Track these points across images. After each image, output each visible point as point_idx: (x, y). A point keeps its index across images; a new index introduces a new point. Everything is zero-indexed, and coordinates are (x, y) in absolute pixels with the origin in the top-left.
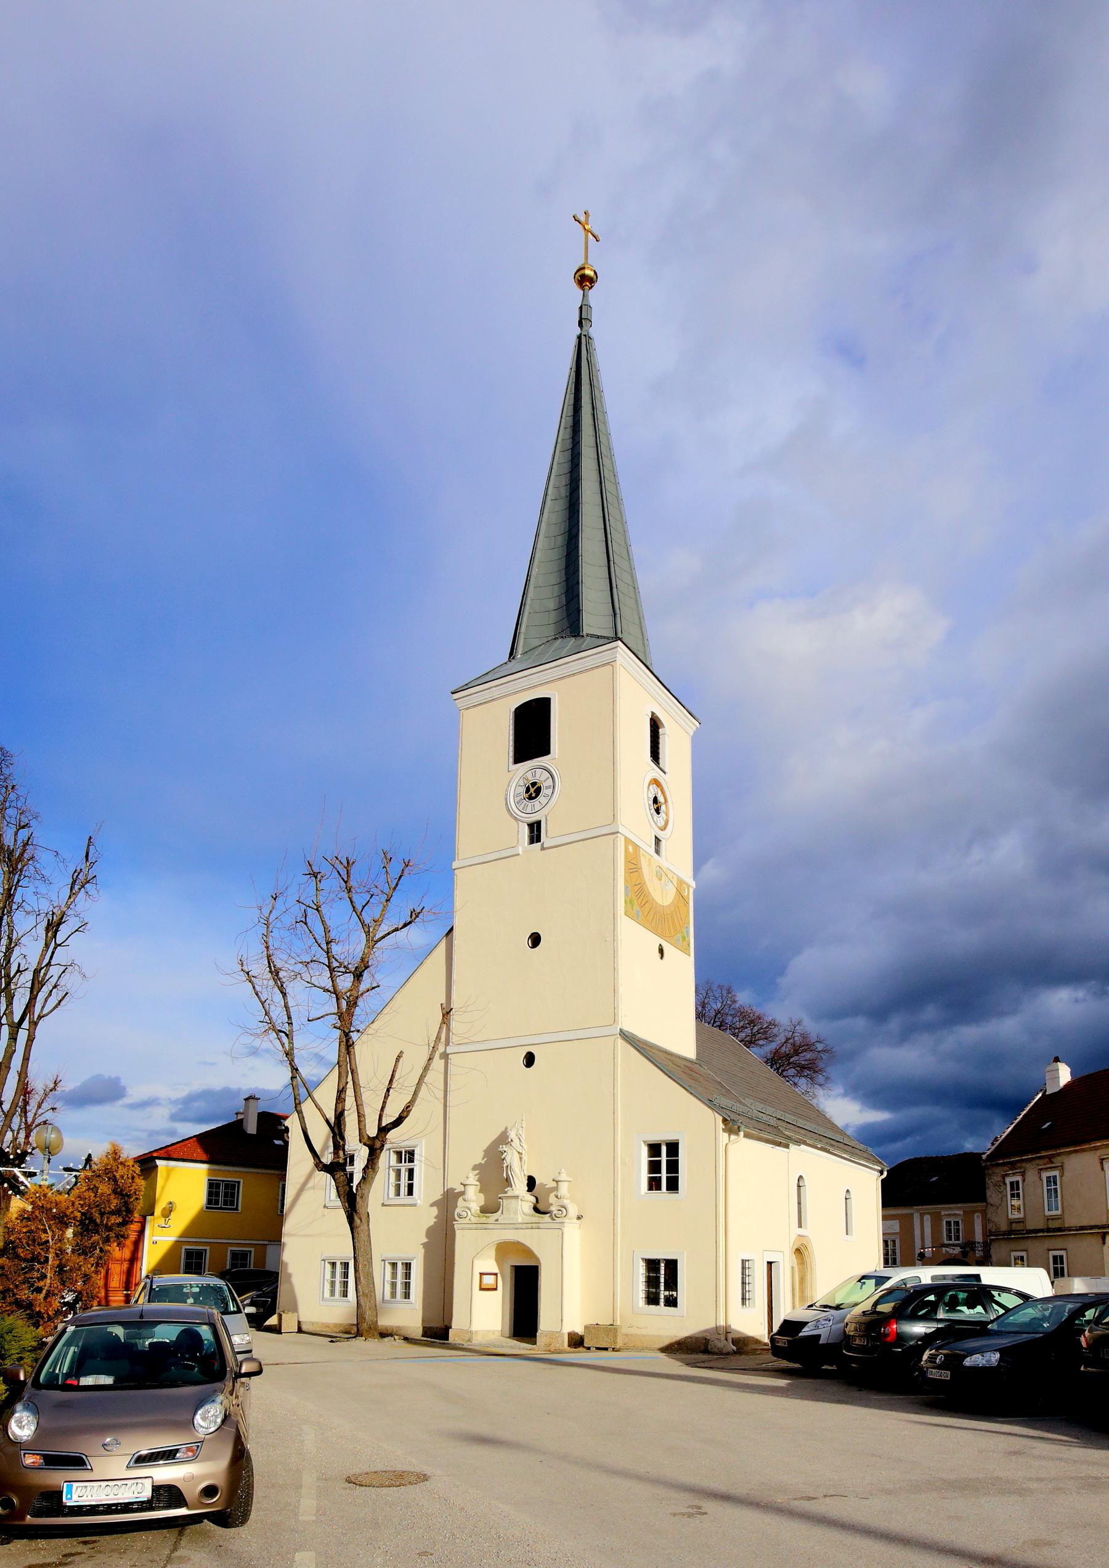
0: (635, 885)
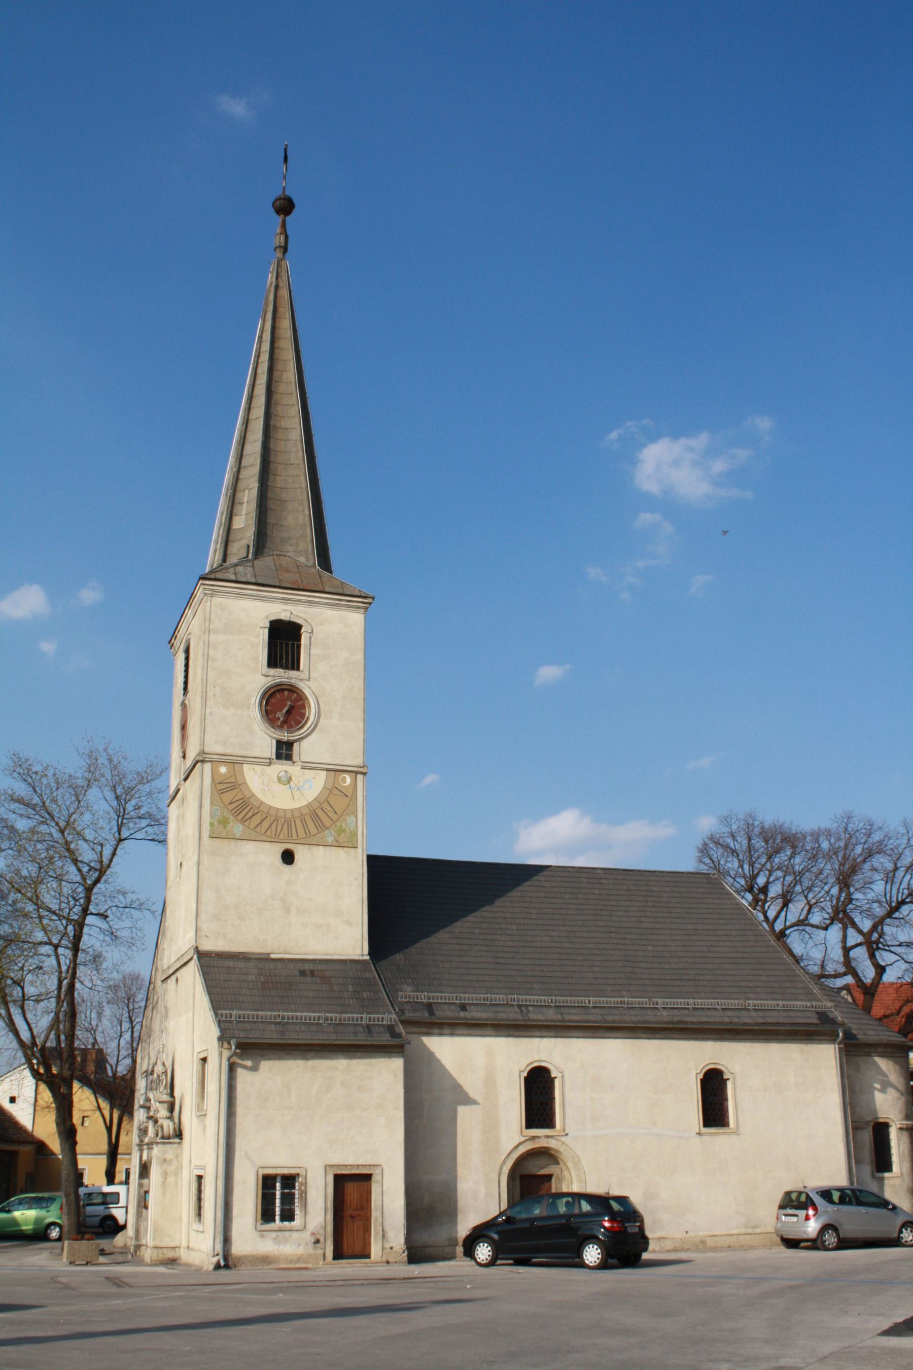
0: (231, 803)
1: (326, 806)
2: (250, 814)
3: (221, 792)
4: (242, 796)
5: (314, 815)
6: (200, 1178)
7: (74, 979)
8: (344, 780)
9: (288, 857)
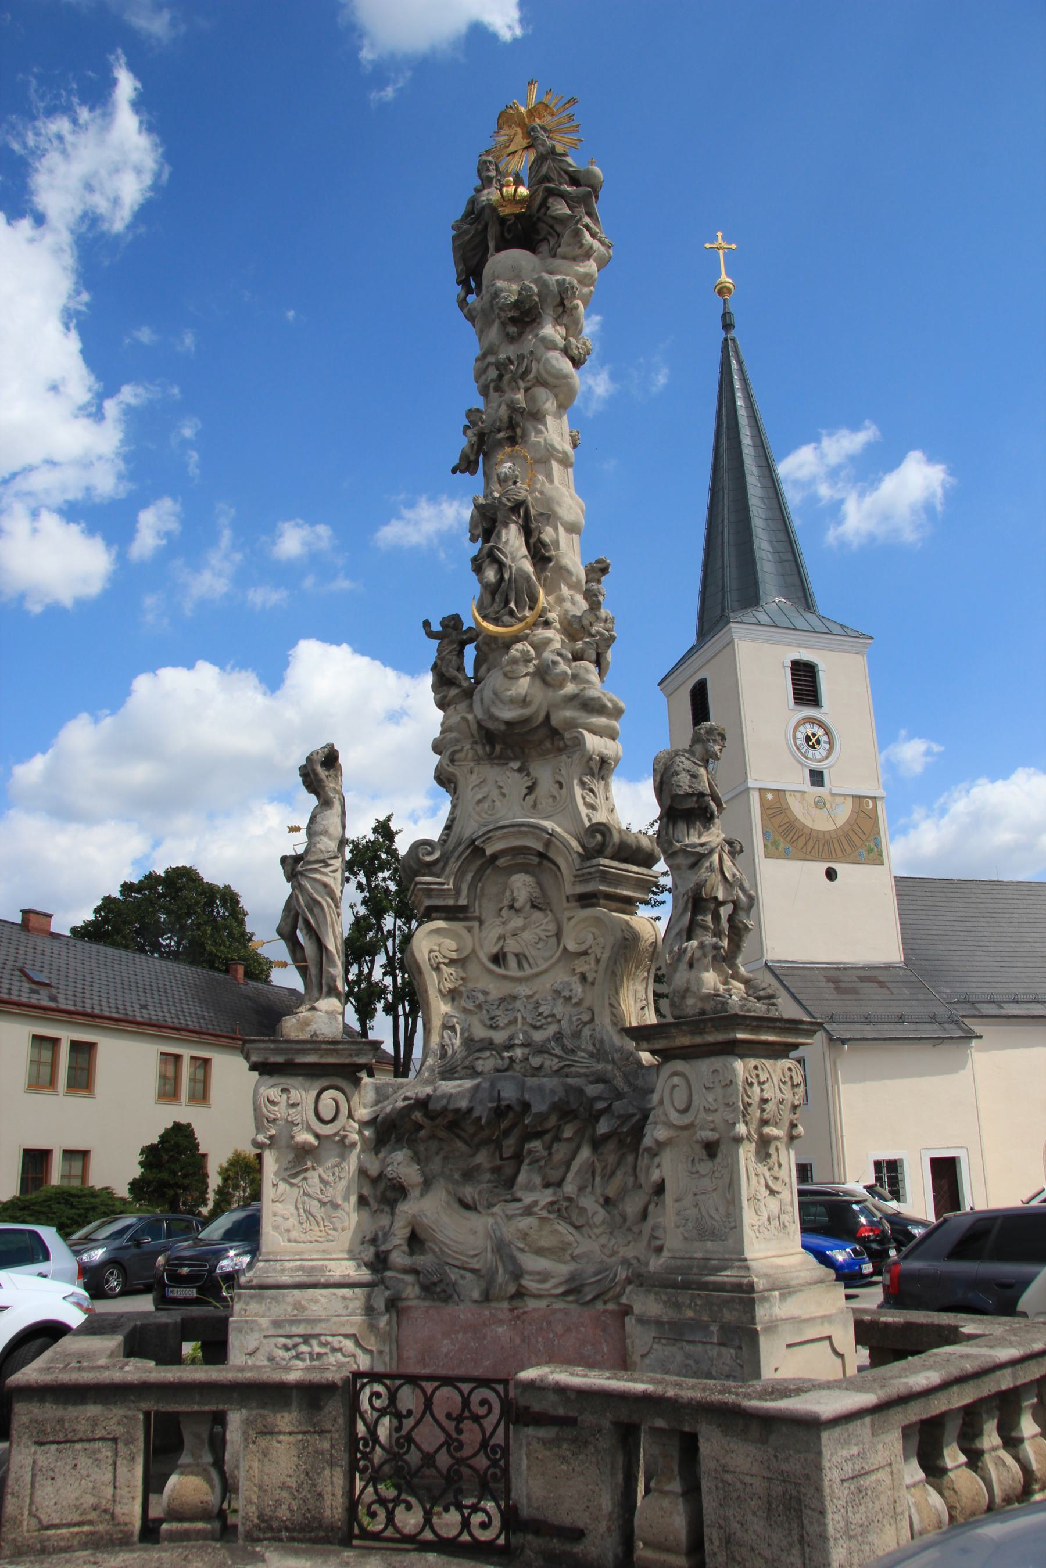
0: (780, 826)
1: (856, 828)
2: (796, 836)
3: (771, 817)
4: (786, 820)
5: (847, 836)
6: (789, 1346)
7: (625, 1339)
8: (867, 804)
9: (831, 874)
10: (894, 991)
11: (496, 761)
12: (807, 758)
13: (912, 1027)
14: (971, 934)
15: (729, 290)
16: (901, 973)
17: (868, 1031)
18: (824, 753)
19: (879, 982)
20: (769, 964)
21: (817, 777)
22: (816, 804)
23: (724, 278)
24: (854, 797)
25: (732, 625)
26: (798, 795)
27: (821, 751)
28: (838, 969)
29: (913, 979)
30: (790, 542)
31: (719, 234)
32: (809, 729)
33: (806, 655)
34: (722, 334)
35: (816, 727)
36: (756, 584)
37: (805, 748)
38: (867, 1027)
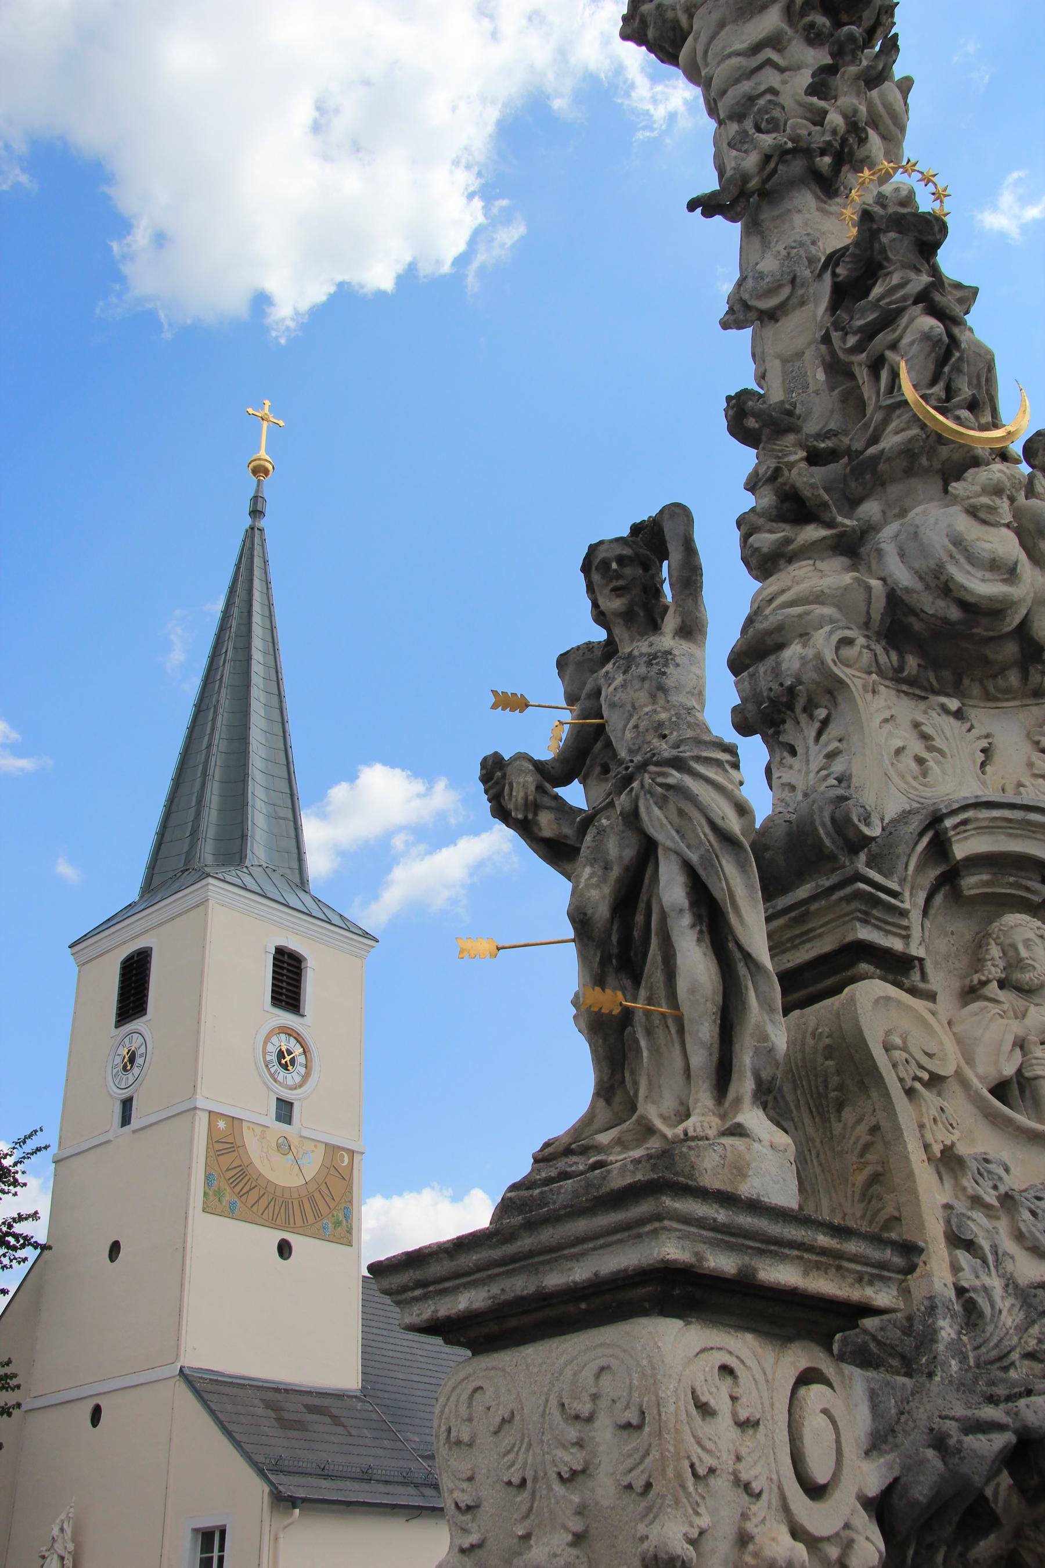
0: (228, 1170)
1: (324, 1188)
2: (247, 1188)
3: (220, 1154)
9: (284, 1249)
10: (354, 1431)
11: (904, 688)
12: (275, 1080)
13: (382, 1488)
14: (435, 1362)
15: (266, 472)
16: (359, 1405)
17: (327, 1489)
18: (298, 1079)
19: (333, 1417)
20: (187, 1371)
21: (285, 1110)
22: (279, 1146)
23: (263, 453)
24: (326, 1144)
25: (210, 880)
26: (258, 1130)
27: (294, 1077)
28: (277, 1390)
29: (374, 1416)
30: (292, 796)
31: (268, 403)
32: (284, 1043)
33: (294, 944)
34: (248, 521)
35: (293, 1041)
36: (243, 837)
37: (275, 1067)
38: (325, 1483)
